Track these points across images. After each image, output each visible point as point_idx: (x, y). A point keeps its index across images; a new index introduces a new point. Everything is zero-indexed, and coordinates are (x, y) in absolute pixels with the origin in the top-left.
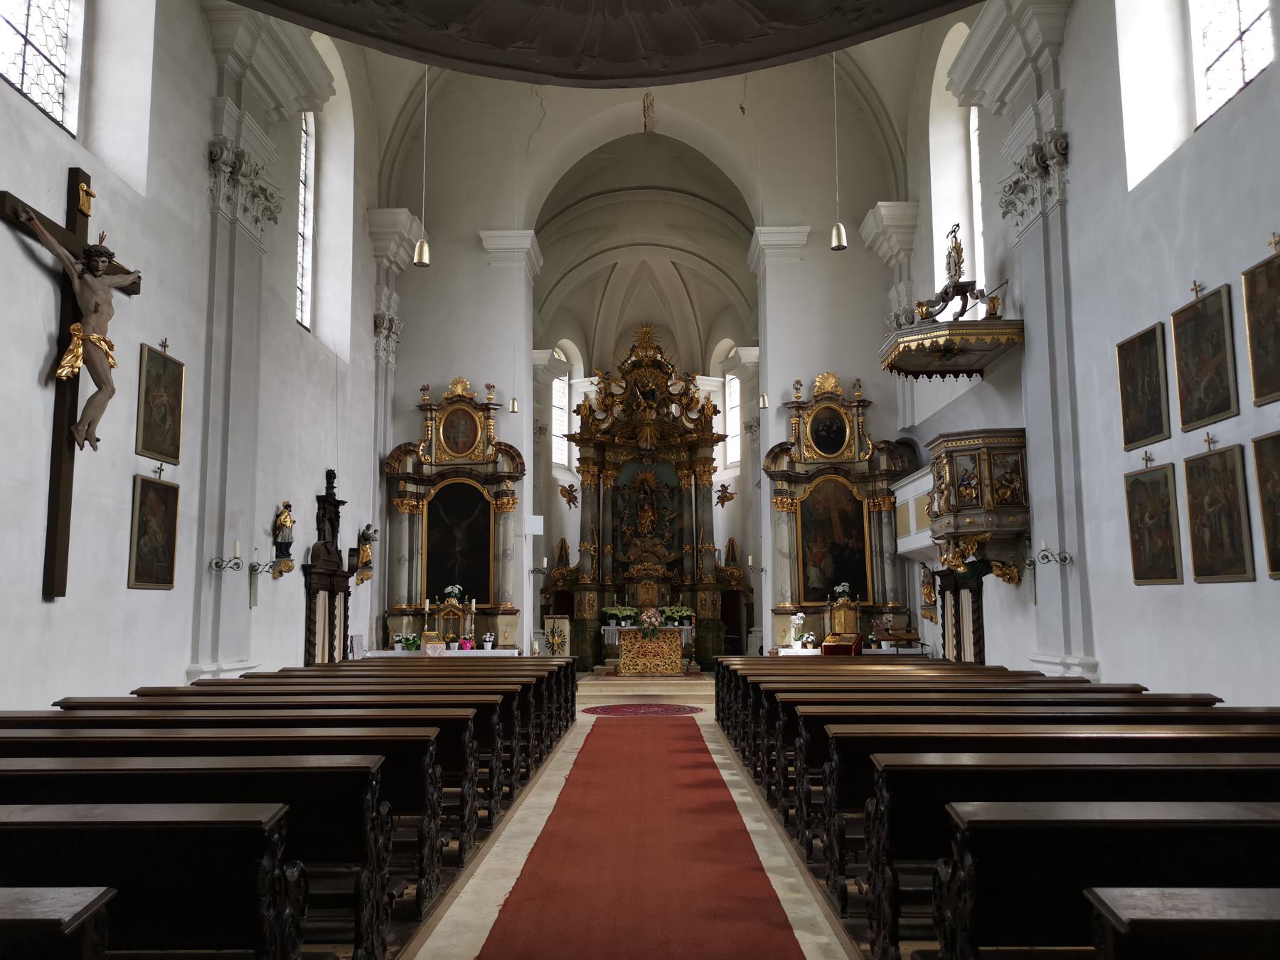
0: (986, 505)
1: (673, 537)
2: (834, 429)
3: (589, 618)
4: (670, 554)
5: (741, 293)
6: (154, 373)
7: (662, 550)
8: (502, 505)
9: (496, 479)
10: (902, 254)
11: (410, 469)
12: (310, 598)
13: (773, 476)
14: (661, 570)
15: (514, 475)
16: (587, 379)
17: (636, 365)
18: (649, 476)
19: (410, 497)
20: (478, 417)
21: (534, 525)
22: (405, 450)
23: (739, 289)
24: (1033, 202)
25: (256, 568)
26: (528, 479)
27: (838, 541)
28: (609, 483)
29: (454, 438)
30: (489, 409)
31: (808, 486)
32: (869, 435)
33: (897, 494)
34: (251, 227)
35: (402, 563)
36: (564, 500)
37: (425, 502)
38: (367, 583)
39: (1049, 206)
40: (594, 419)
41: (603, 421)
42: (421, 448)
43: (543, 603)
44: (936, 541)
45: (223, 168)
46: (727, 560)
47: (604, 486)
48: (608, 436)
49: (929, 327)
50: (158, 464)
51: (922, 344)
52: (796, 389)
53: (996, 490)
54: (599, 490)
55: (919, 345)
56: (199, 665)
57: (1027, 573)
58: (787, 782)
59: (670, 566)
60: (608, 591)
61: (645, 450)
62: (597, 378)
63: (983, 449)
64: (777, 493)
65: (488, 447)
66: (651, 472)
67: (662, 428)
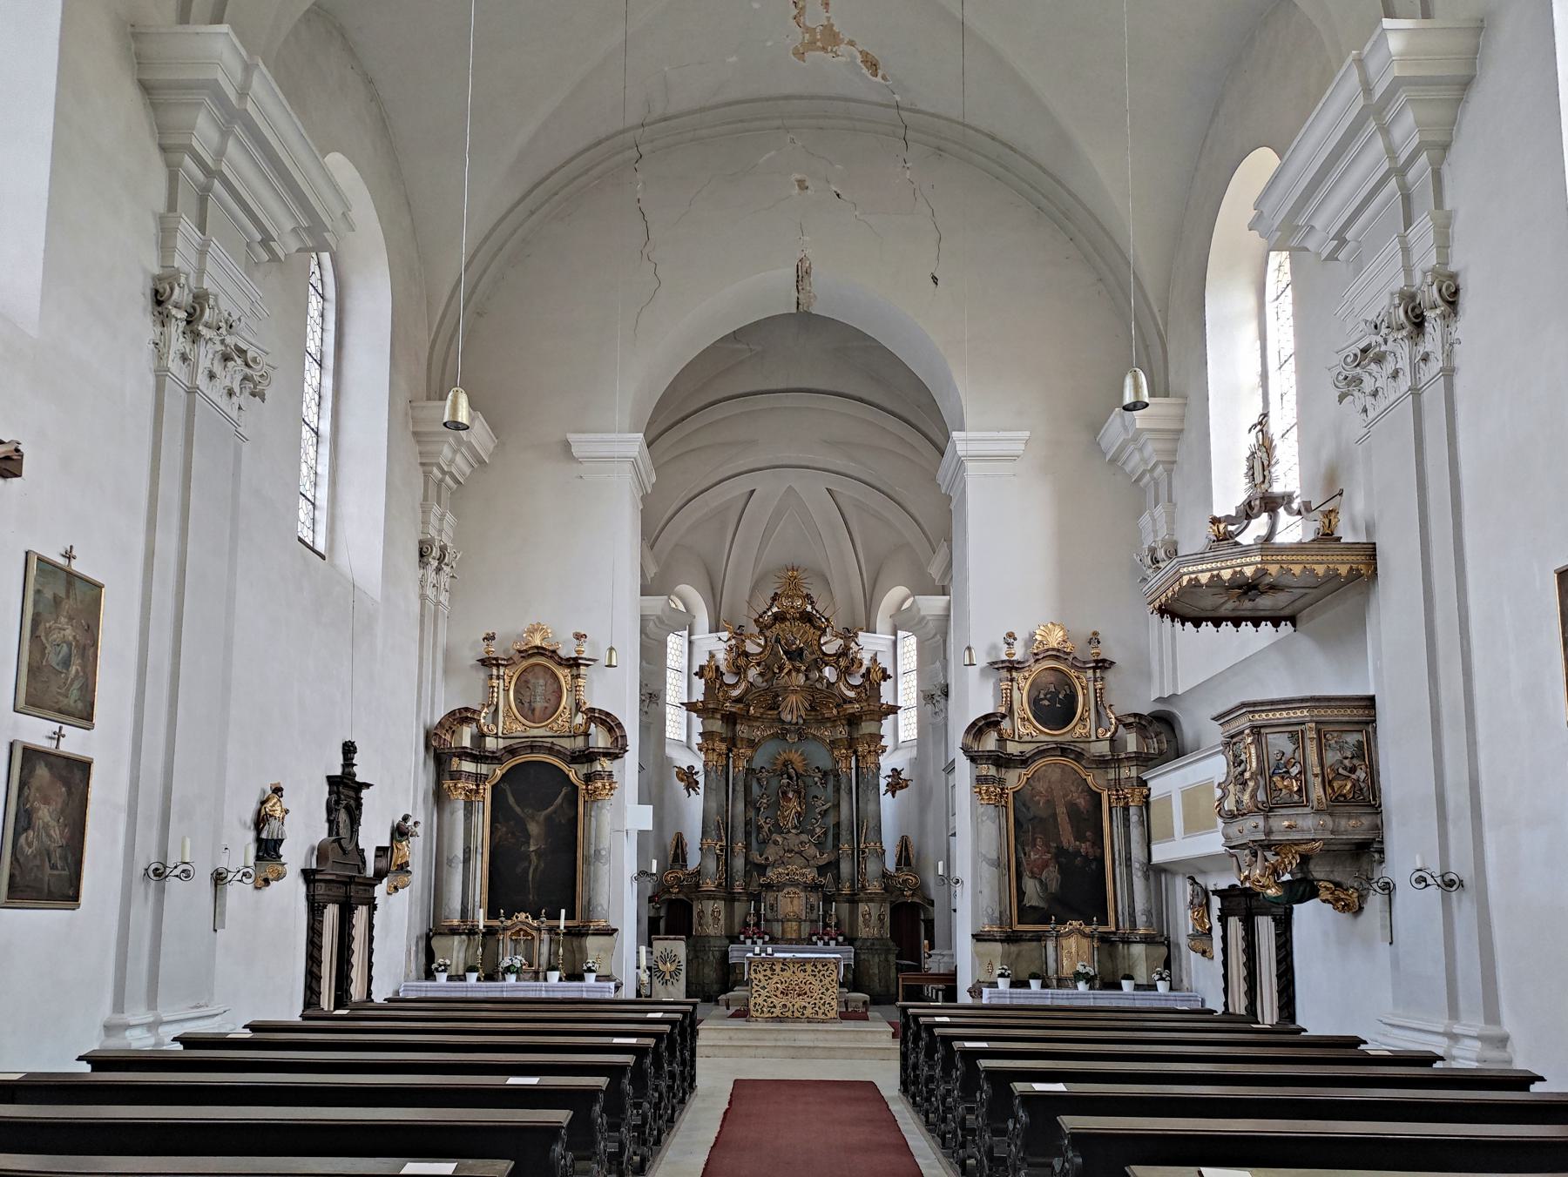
0: (1315, 803)
1: (825, 833)
2: (1061, 696)
3: (713, 934)
4: (822, 854)
5: (922, 529)
6: (48, 594)
7: (811, 851)
8: (595, 792)
9: (587, 756)
10: (1160, 468)
11: (467, 742)
12: (314, 915)
13: (974, 759)
14: (811, 874)
15: (611, 751)
16: (714, 635)
17: (779, 618)
18: (795, 757)
19: (467, 779)
20: (563, 674)
21: (642, 817)
22: (462, 716)
23: (919, 524)
24: (1395, 375)
25: (224, 875)
26: (632, 758)
27: (1065, 845)
28: (741, 764)
29: (530, 702)
30: (578, 665)
31: (1023, 771)
32: (1111, 705)
33: (1150, 784)
34: (223, 402)
35: (453, 865)
36: (682, 785)
37: (488, 786)
38: (404, 893)
39: (1422, 377)
40: (723, 684)
41: (734, 686)
42: (483, 714)
43: (651, 915)
44: (1231, 851)
45: (174, 311)
46: (899, 863)
47: (734, 768)
48: (741, 706)
49: (1230, 551)
50: (56, 726)
51: (1218, 575)
52: (1008, 644)
53: (1330, 782)
54: (728, 773)
55: (1212, 576)
56: (125, 1015)
57: (1375, 901)
58: (965, 1133)
59: (822, 870)
60: (738, 900)
61: (790, 723)
62: (727, 633)
63: (1309, 724)
64: (980, 780)
65: (576, 715)
66: (796, 751)
67: (813, 696)
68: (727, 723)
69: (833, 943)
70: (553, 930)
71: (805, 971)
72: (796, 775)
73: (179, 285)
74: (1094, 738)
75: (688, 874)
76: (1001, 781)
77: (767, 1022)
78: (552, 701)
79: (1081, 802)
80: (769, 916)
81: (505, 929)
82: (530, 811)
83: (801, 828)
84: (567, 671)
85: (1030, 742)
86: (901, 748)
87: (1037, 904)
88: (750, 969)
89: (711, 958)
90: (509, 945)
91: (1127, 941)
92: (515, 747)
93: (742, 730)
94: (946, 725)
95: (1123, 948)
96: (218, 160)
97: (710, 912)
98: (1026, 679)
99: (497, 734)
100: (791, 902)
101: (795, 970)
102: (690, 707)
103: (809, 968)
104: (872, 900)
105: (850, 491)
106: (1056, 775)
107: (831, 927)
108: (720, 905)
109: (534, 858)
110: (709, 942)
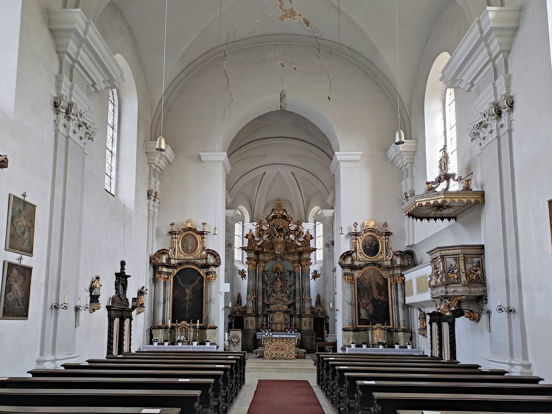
0: (463, 283)
1: (290, 293)
2: (373, 245)
3: (251, 328)
4: (289, 300)
5: (324, 186)
6: (17, 209)
7: (286, 299)
8: (209, 278)
9: (207, 266)
10: (408, 165)
11: (164, 261)
12: (110, 322)
13: (343, 267)
14: (285, 308)
15: (215, 264)
16: (251, 223)
17: (274, 217)
18: (280, 266)
19: (164, 274)
20: (198, 237)
21: (226, 288)
22: (163, 252)
23: (323, 184)
24: (491, 132)
25: (79, 308)
26: (222, 267)
27: (375, 297)
28: (261, 269)
29: (187, 247)
30: (204, 234)
31: (360, 271)
32: (391, 248)
33: (405, 276)
34: (78, 141)
35: (159, 304)
36: (240, 276)
37: (172, 277)
38: (142, 314)
39: (501, 133)
40: (254, 241)
41: (258, 241)
42: (170, 251)
43: (229, 322)
44: (433, 299)
45: (61, 110)
46: (316, 303)
47: (258, 270)
48: (261, 248)
49: (433, 194)
50: (20, 256)
51: (429, 202)
52: (355, 226)
53: (468, 275)
54: (256, 272)
55: (427, 203)
57: (484, 317)
58: (340, 398)
59: (289, 306)
60: (260, 317)
61: (278, 254)
62: (256, 223)
63: (461, 255)
64: (345, 274)
65: (203, 251)
66: (280, 264)
67: (286, 245)
68: (256, 254)
69: (293, 332)
70: (195, 327)
71: (283, 342)
72: (280, 273)
73: (63, 100)
74: (385, 260)
75: (242, 308)
76: (352, 275)
77: (270, 359)
78: (194, 247)
79: (381, 282)
80: (271, 322)
81: (178, 327)
82: (187, 285)
83: (282, 291)
84: (200, 236)
85: (363, 261)
86: (317, 263)
87: (365, 318)
88: (264, 341)
89: (250, 337)
90: (179, 332)
91: (397, 331)
92: (181, 263)
93: (261, 257)
94: (333, 255)
95: (395, 333)
96: (77, 56)
97: (250, 321)
98: (361, 239)
99: (175, 258)
100: (279, 317)
101: (280, 341)
102: (243, 249)
103: (285, 340)
104: (307, 317)
105: (299, 173)
106: (372, 273)
107: (292, 326)
108: (254, 318)
109: (188, 302)
110: (250, 331)
